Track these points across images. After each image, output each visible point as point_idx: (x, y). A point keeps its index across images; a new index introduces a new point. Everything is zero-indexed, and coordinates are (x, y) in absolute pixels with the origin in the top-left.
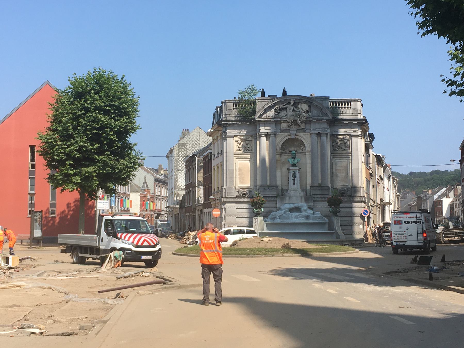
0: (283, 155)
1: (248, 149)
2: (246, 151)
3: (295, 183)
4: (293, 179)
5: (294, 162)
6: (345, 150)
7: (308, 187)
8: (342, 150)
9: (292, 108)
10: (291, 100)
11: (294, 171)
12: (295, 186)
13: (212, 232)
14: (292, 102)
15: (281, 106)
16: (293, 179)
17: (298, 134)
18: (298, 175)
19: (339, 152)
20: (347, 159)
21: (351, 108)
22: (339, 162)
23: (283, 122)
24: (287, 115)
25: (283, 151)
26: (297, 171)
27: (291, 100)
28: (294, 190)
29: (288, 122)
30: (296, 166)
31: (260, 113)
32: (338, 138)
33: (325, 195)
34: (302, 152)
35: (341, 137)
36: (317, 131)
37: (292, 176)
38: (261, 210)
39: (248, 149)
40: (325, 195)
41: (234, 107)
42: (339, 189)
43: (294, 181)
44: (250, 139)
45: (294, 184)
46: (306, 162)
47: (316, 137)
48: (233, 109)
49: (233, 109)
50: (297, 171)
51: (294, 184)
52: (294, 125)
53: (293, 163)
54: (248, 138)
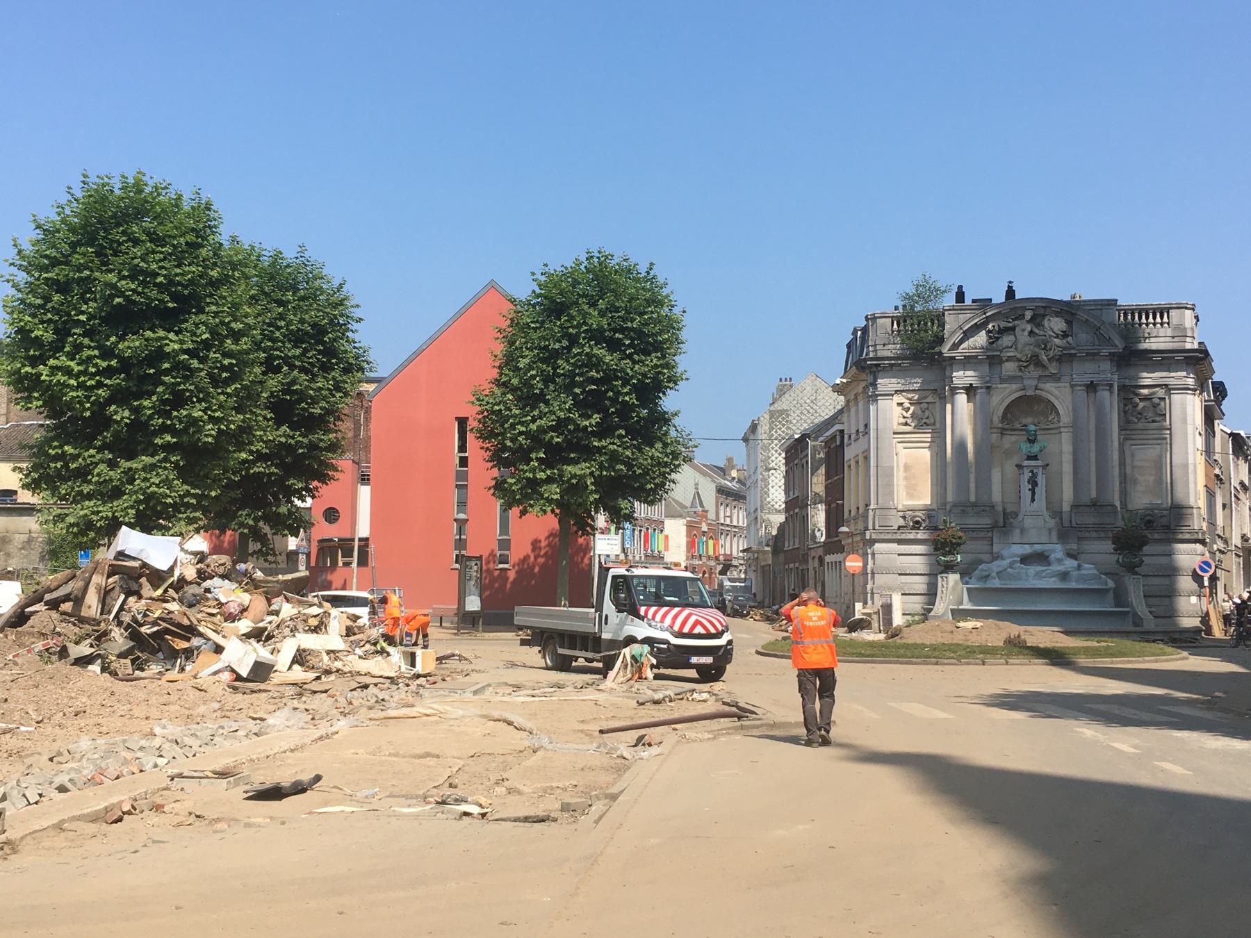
3: (1036, 498)
4: (1029, 490)
6: (1153, 421)
11: (1032, 472)
14: (1028, 315)
16: (1029, 490)
17: (1041, 385)
19: (1140, 425)
21: (1168, 324)
23: (1007, 361)
24: (1015, 343)
27: (1025, 308)
29: (1020, 360)
36: (1087, 379)
37: (1029, 482)
45: (1033, 500)
51: (1033, 500)
52: (1032, 366)
54: (926, 397)
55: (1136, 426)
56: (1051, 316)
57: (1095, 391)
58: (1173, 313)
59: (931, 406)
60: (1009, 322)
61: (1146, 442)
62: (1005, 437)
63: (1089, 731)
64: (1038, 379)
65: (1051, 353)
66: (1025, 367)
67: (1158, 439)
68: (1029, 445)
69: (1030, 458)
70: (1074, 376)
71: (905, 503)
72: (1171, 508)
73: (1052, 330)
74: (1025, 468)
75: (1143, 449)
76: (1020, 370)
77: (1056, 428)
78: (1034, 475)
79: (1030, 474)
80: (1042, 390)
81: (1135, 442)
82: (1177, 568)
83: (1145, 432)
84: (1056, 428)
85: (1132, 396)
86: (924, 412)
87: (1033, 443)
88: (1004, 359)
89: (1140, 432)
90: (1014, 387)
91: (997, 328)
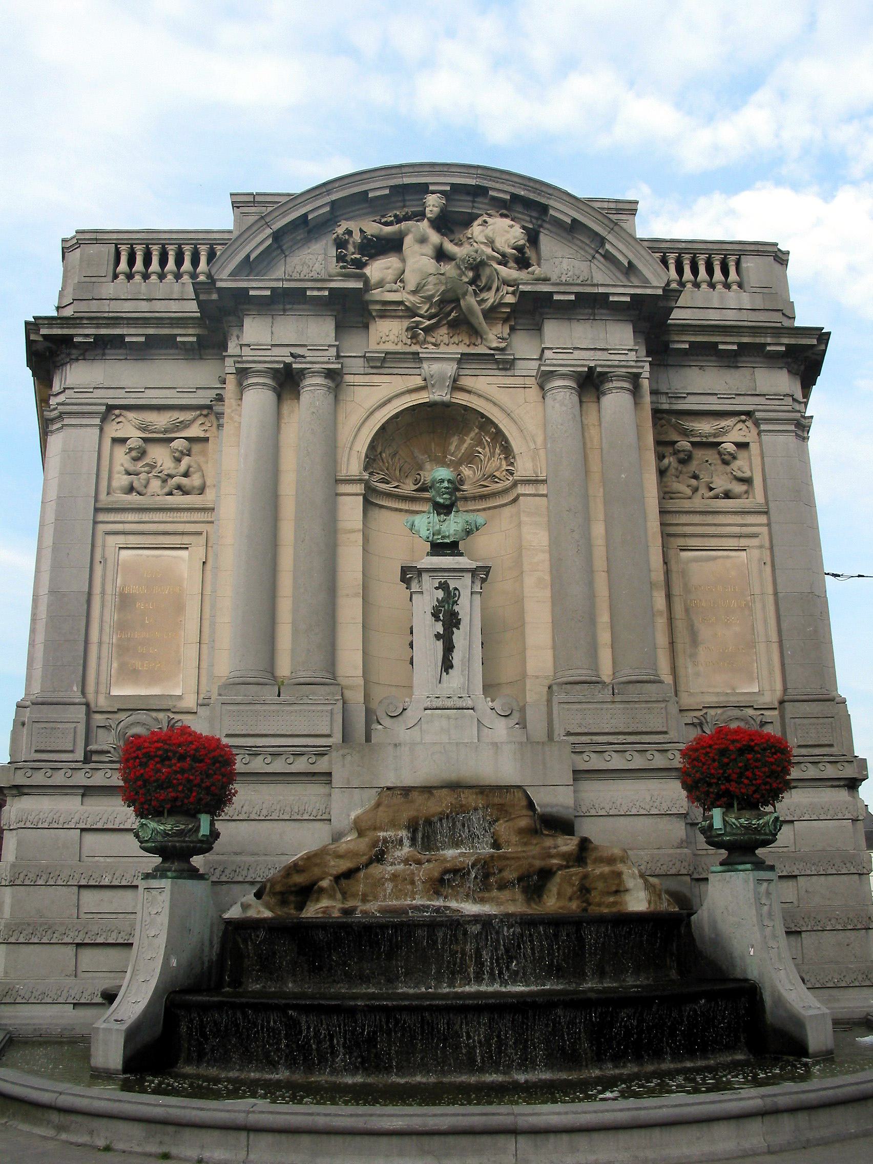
0: (382, 507)
1: (184, 481)
2: (170, 494)
3: (455, 662)
4: (438, 636)
5: (444, 528)
6: (727, 495)
7: (534, 693)
8: (716, 497)
9: (435, 238)
10: (424, 189)
11: (443, 586)
12: (454, 680)
13: (590, 840)
14: (433, 203)
15: (372, 228)
16: (438, 636)
17: (466, 382)
18: (465, 607)
19: (697, 503)
20: (743, 542)
21: (740, 286)
22: (696, 560)
23: (383, 315)
24: (400, 278)
25: (383, 481)
26: (464, 584)
27: (424, 189)
28: (449, 703)
29: (411, 312)
30: (461, 555)
31: (254, 285)
32: (685, 433)
33: (646, 739)
34: (500, 486)
35: (705, 427)
36: (585, 360)
37: (435, 615)
38: (198, 829)
39: (184, 481)
40: (646, 739)
41: (123, 266)
42: (712, 712)
43: (449, 648)
44: (195, 431)
45: (447, 665)
46: (520, 537)
47: (575, 398)
48: (116, 276)
49: (116, 276)
50: (464, 584)
51: (447, 665)
52: (444, 330)
53: (439, 532)
54: (185, 425)
55: (686, 505)
56: (490, 215)
57: (599, 394)
58: (748, 263)
59: (196, 448)
60: (386, 224)
61: (713, 542)
62: (375, 513)
63: (107, 469)
64: (459, 361)
65: (490, 298)
66: (427, 330)
67: (740, 536)
68: (435, 518)
69: (439, 548)
70: (548, 354)
71: (115, 692)
72: (782, 702)
73: (491, 243)
74: (425, 577)
75: (715, 558)
76: (414, 337)
77: (505, 491)
78: (450, 596)
79: (440, 594)
80: (469, 392)
81: (692, 542)
82: (355, 1075)
83: (710, 519)
84: (505, 491)
85: (674, 437)
86: (178, 460)
87: (448, 513)
88: (374, 314)
89: (697, 519)
90: (397, 383)
91: (357, 237)
